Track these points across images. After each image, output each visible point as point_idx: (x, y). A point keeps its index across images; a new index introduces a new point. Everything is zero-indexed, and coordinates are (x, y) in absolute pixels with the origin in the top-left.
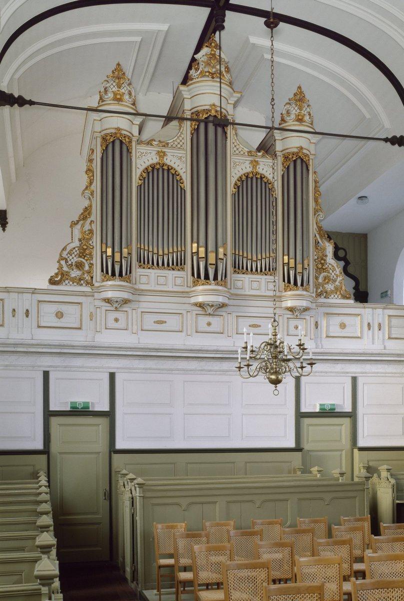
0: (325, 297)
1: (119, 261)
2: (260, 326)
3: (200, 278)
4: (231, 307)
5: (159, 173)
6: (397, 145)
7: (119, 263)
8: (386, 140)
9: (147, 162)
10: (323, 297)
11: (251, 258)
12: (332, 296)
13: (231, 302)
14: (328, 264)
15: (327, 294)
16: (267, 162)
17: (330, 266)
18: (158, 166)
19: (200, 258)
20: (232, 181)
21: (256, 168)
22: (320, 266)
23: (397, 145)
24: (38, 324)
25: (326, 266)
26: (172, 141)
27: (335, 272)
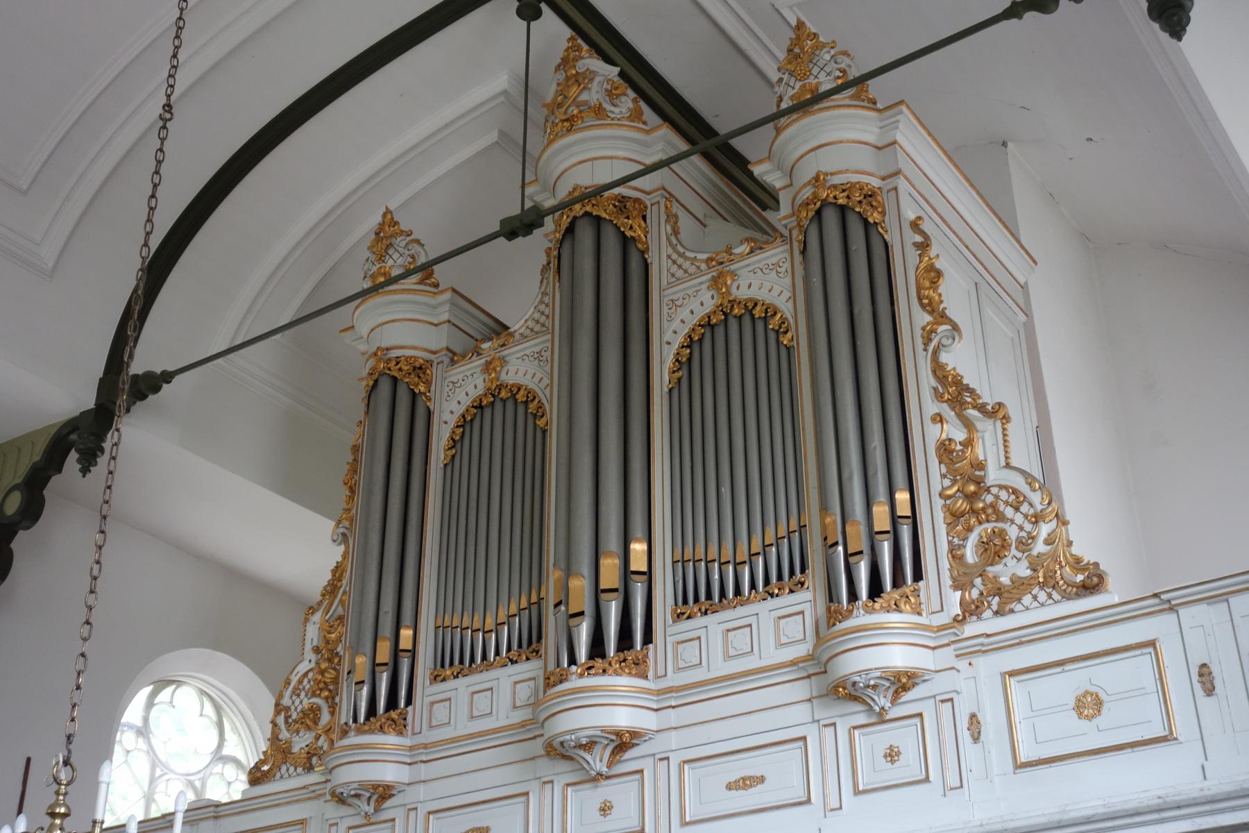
0: (996, 613)
1: (909, 514)
2: (762, 779)
3: (603, 656)
4: (659, 736)
5: (503, 405)
6: (165, 386)
7: (910, 521)
8: (167, 377)
9: (521, 374)
10: (988, 614)
11: (410, 647)
12: (1027, 599)
13: (423, 771)
14: (994, 490)
15: (1007, 597)
16: (759, 261)
17: (1004, 495)
18: (503, 394)
19: (605, 591)
20: (665, 353)
21: (729, 292)
22: (961, 504)
23: (165, 386)
24: (1155, 648)
25: (989, 499)
26: (522, 322)
27: (1025, 508)
